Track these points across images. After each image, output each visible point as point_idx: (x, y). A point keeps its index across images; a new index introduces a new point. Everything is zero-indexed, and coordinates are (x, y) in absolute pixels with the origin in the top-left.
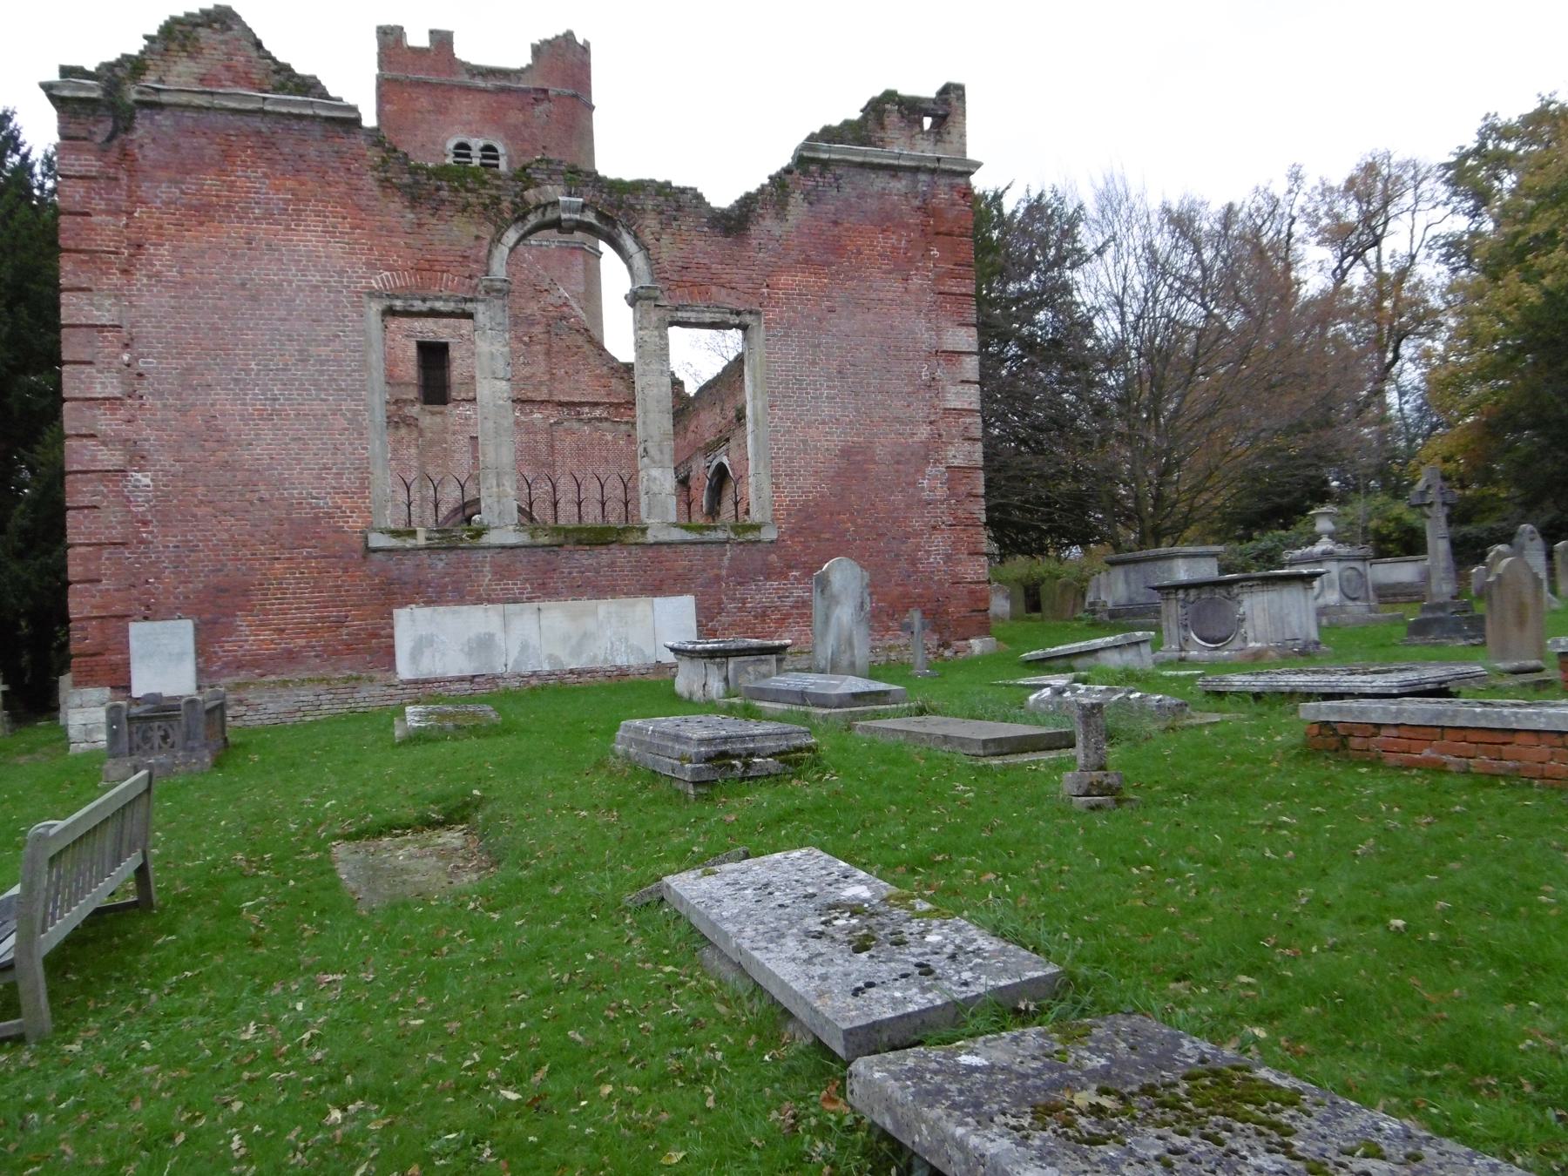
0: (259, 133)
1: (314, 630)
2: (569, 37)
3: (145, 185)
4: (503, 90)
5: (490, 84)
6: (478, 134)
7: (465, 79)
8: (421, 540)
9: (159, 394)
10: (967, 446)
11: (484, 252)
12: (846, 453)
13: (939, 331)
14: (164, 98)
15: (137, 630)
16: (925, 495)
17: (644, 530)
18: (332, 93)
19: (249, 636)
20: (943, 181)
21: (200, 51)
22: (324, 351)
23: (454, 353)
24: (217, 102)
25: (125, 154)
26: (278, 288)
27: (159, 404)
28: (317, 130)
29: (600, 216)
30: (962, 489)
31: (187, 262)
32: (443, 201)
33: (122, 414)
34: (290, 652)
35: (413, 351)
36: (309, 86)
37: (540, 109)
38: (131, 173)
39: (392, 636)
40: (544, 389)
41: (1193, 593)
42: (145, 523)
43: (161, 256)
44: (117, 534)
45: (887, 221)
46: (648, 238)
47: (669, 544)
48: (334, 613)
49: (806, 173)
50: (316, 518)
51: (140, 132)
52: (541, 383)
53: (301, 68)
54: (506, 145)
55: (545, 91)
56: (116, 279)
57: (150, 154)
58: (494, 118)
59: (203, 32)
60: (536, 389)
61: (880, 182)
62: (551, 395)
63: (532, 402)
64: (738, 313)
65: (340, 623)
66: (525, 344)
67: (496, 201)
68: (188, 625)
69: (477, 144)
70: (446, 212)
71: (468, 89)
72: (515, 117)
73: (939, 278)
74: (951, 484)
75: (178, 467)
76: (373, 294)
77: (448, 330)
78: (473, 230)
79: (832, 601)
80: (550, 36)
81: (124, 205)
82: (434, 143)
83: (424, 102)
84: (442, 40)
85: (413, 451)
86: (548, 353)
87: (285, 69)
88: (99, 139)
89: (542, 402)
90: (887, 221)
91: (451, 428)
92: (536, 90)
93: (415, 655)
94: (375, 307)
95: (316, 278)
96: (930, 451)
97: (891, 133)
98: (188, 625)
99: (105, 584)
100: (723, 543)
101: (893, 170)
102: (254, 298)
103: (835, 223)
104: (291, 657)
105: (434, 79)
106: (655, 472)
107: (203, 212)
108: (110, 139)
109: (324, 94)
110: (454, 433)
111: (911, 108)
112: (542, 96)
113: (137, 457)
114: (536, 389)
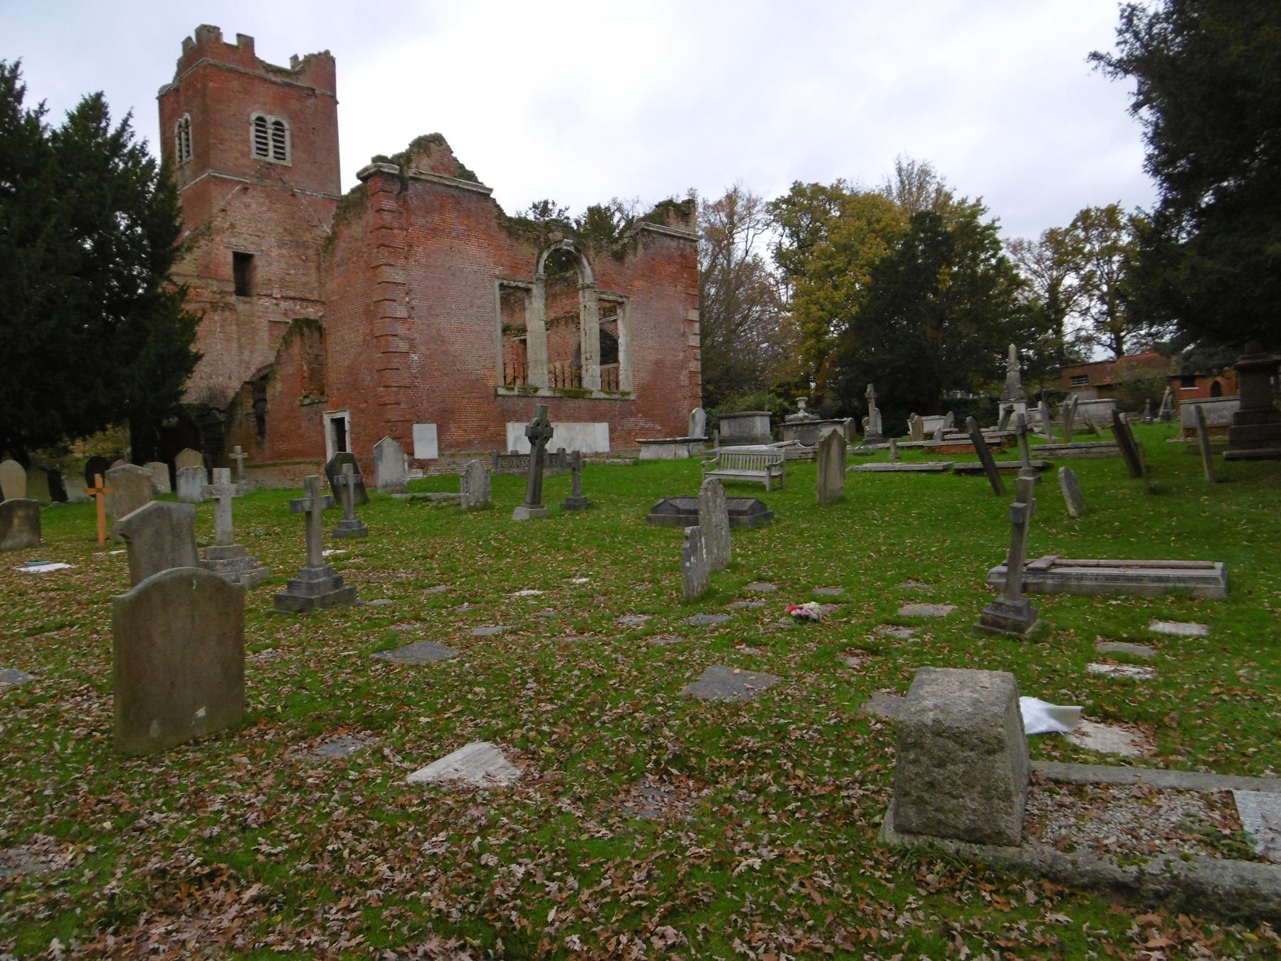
0: (453, 196)
1: (478, 431)
2: (327, 53)
3: (413, 217)
4: (287, 85)
5: (278, 79)
6: (271, 113)
7: (262, 72)
8: (516, 392)
9: (420, 317)
10: (696, 362)
11: (535, 261)
12: (657, 363)
13: (686, 310)
14: (423, 177)
15: (416, 427)
16: (682, 383)
17: (591, 392)
18: (480, 180)
19: (455, 433)
20: (688, 243)
21: (431, 153)
22: (479, 302)
23: (259, 262)
24: (442, 181)
25: (405, 202)
26: (462, 270)
27: (420, 322)
28: (474, 197)
29: (576, 248)
30: (693, 382)
31: (429, 256)
32: (520, 236)
33: (406, 326)
34: (469, 440)
35: (230, 258)
36: (471, 176)
37: (312, 101)
38: (408, 211)
39: (505, 435)
40: (316, 292)
41: (799, 428)
42: (416, 378)
43: (419, 251)
44: (407, 382)
45: (670, 260)
46: (591, 260)
47: (599, 399)
48: (483, 423)
49: (643, 235)
50: (477, 380)
51: (411, 191)
52: (314, 288)
53: (468, 168)
54: (289, 123)
55: (313, 90)
56: (403, 261)
57: (414, 202)
58: (281, 103)
59: (432, 145)
60: (311, 292)
61: (667, 242)
62: (320, 297)
63: (307, 300)
64: (621, 297)
65: (487, 428)
66: (304, 261)
67: (539, 237)
68: (434, 426)
69: (270, 119)
70: (521, 241)
71: (265, 80)
72: (295, 105)
73: (687, 287)
74: (690, 378)
75: (428, 353)
76: (497, 277)
77: (253, 246)
78: (531, 250)
79: (695, 425)
80: (316, 52)
81: (405, 226)
82: (242, 114)
83: (235, 84)
84: (246, 43)
85: (234, 327)
86: (318, 268)
87: (462, 167)
88: (395, 193)
89: (313, 301)
90: (670, 260)
91: (257, 314)
92: (308, 88)
93: (515, 443)
94: (497, 283)
95: (475, 268)
96: (682, 365)
97: (671, 220)
98: (434, 426)
99: (403, 406)
100: (616, 400)
101: (672, 237)
102: (453, 275)
103: (653, 259)
104: (470, 443)
105: (242, 69)
106: (594, 367)
107: (434, 232)
108: (400, 193)
109: (476, 181)
110: (259, 317)
111: (677, 207)
112: (310, 93)
113: (413, 348)
114: (311, 292)
